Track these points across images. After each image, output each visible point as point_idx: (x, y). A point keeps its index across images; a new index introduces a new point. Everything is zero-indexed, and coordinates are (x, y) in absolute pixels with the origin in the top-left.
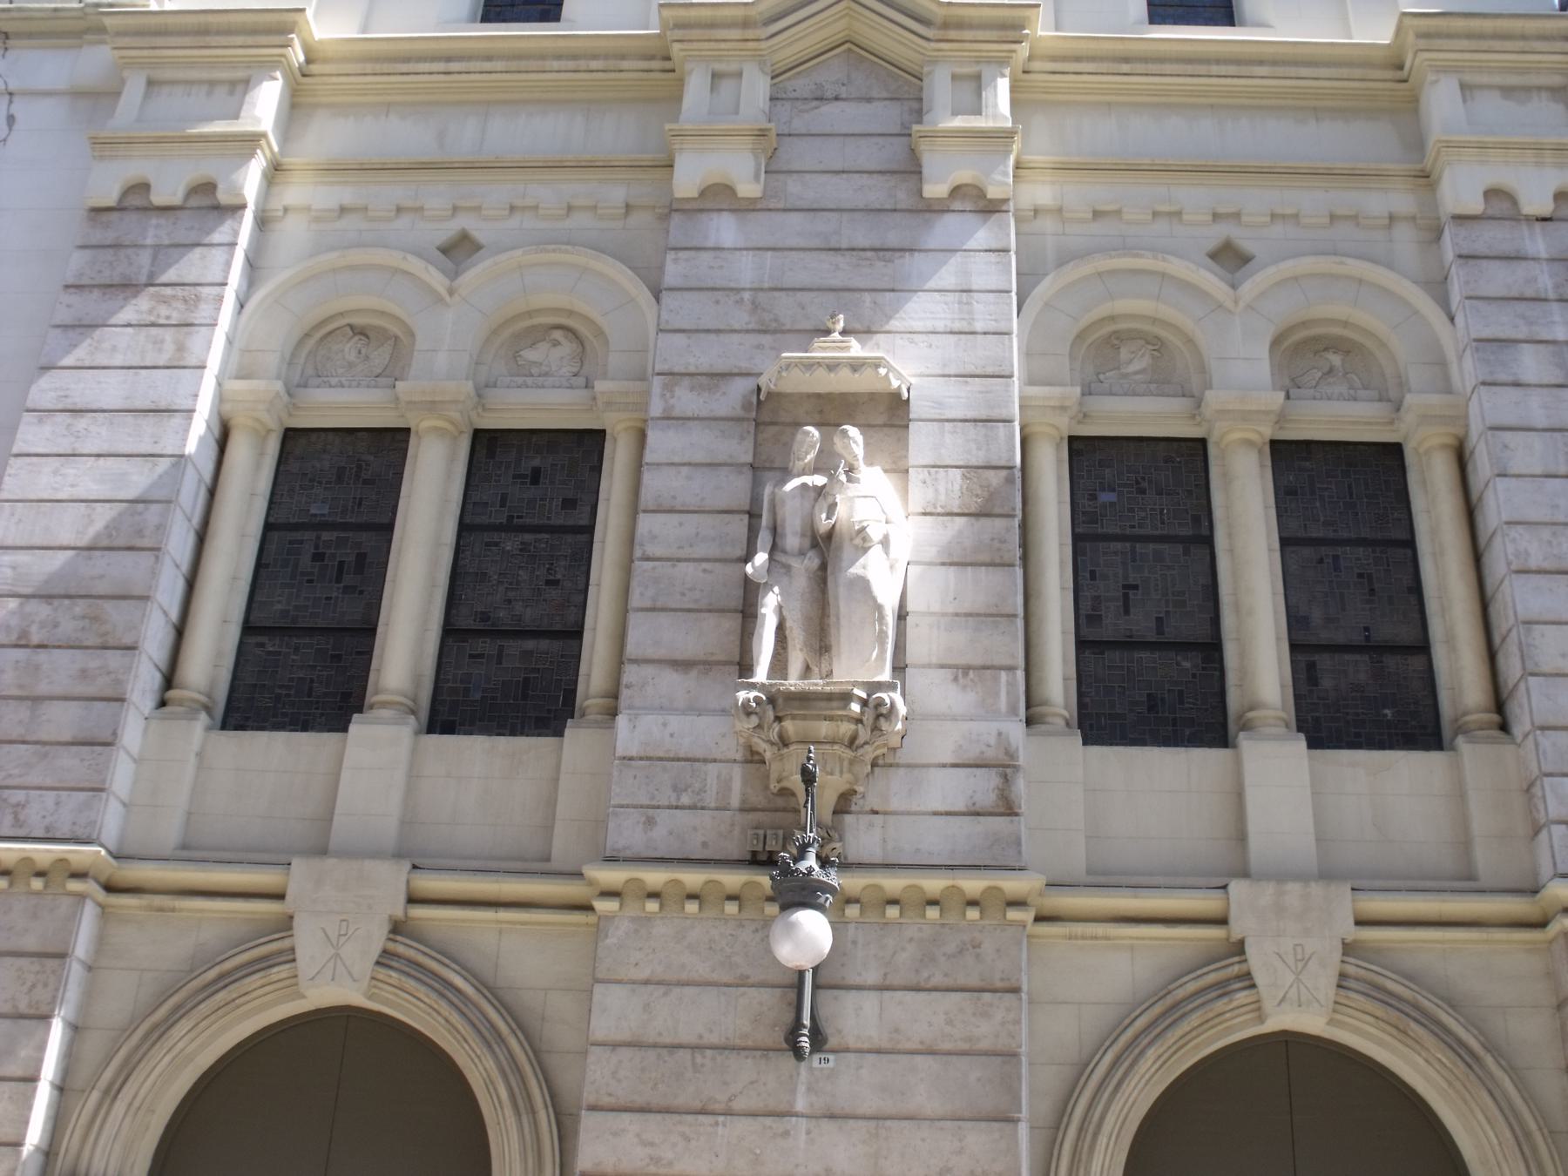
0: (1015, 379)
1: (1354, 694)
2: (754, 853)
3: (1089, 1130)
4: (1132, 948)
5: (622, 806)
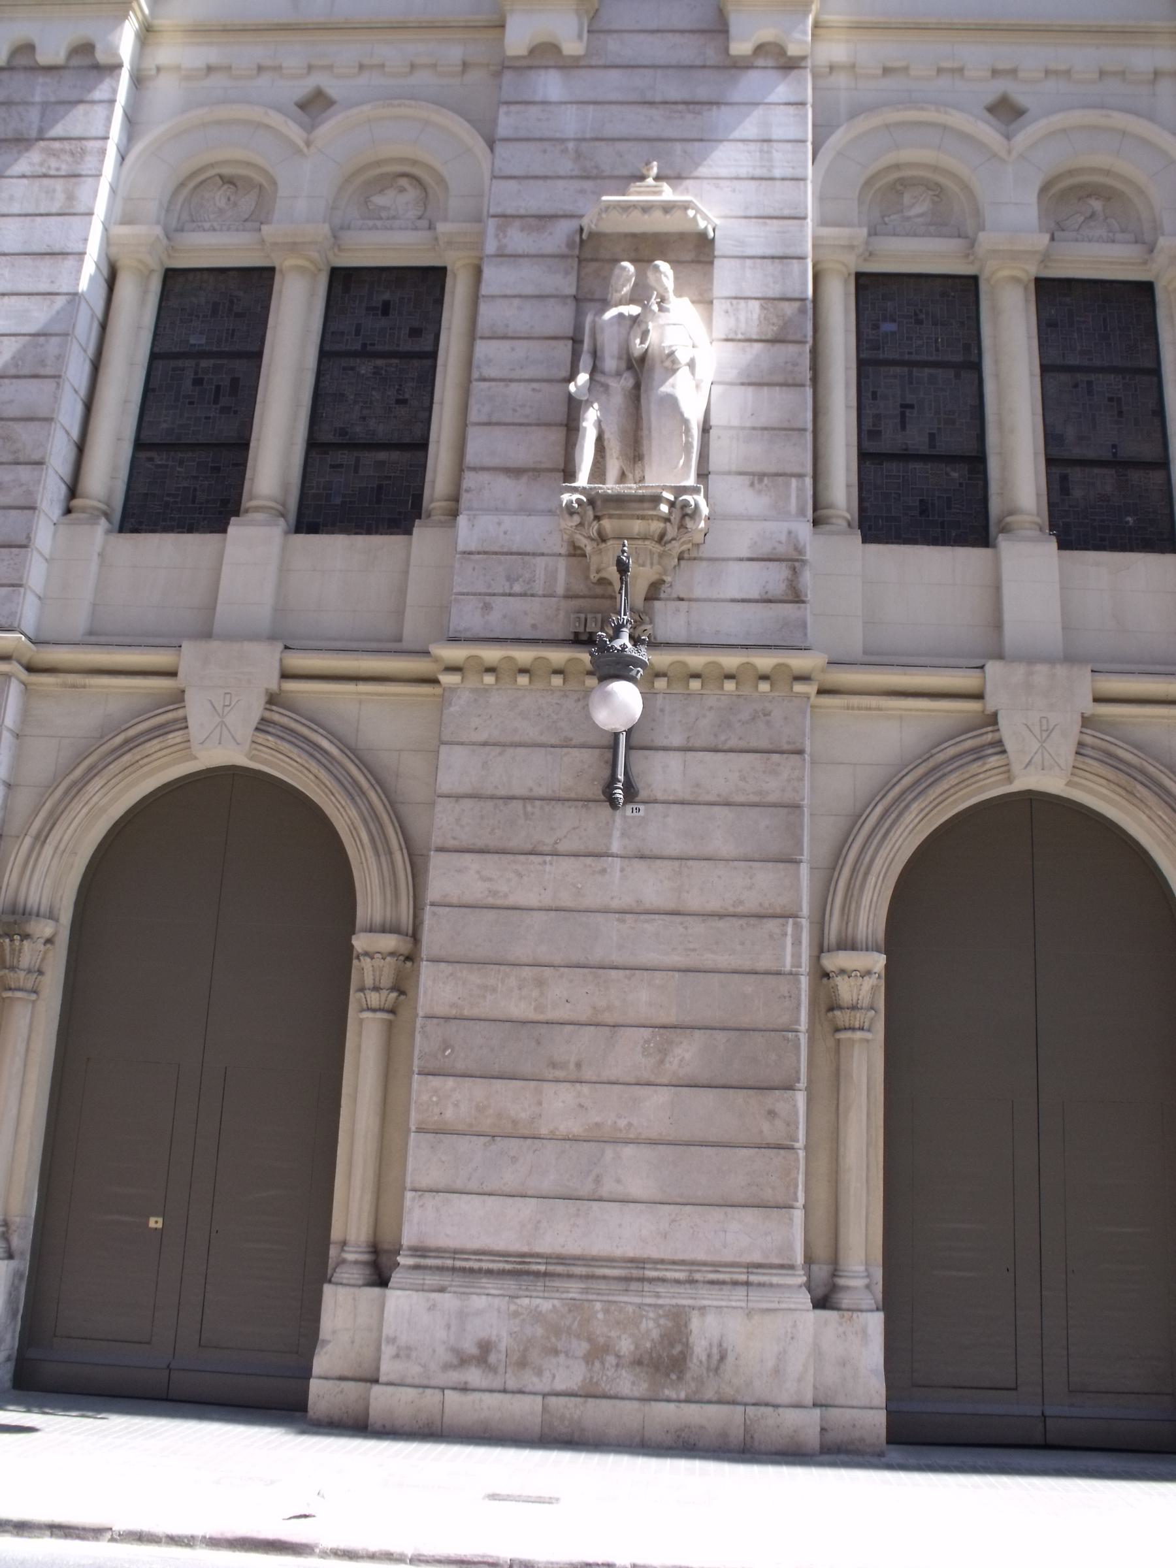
0: (809, 220)
1: (1100, 503)
2: (576, 634)
3: (860, 872)
4: (901, 718)
5: (463, 594)
